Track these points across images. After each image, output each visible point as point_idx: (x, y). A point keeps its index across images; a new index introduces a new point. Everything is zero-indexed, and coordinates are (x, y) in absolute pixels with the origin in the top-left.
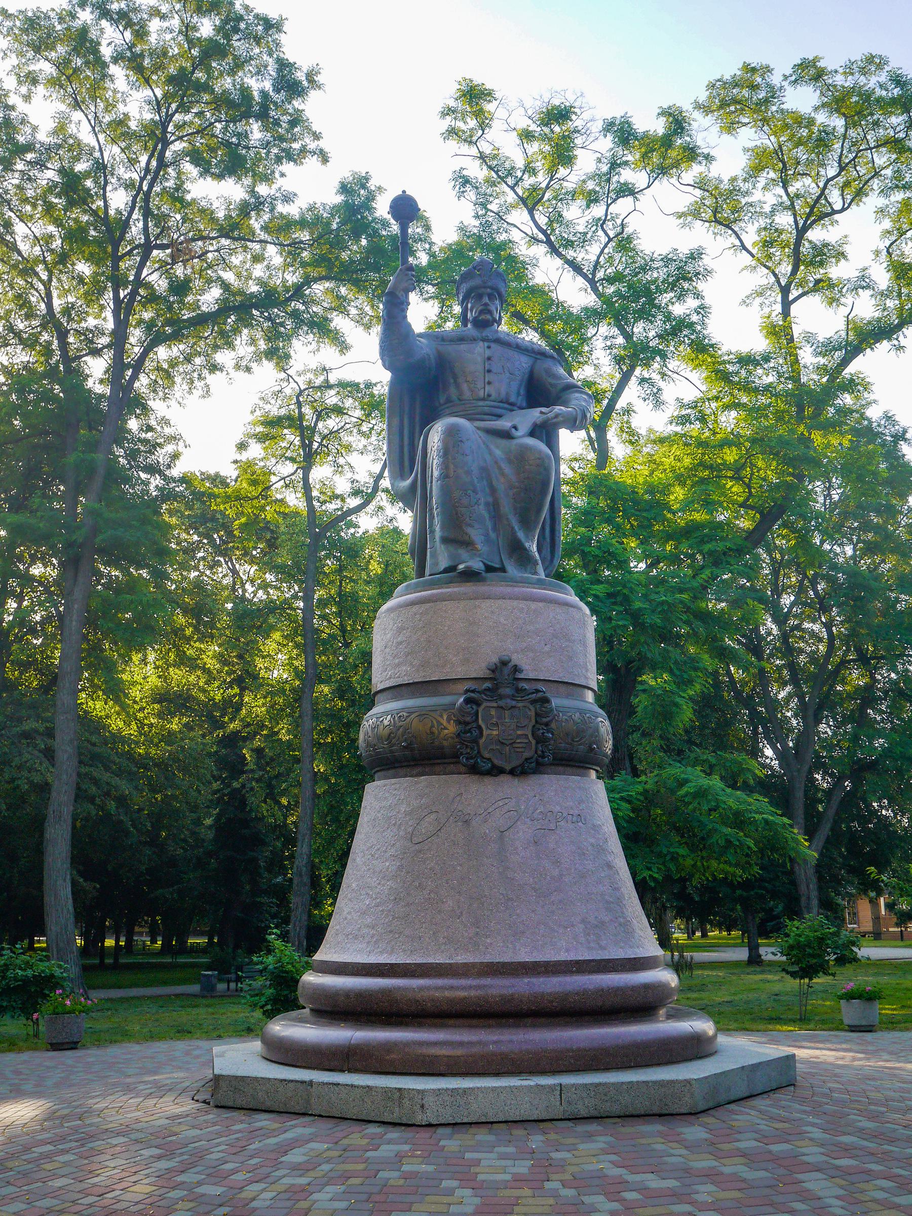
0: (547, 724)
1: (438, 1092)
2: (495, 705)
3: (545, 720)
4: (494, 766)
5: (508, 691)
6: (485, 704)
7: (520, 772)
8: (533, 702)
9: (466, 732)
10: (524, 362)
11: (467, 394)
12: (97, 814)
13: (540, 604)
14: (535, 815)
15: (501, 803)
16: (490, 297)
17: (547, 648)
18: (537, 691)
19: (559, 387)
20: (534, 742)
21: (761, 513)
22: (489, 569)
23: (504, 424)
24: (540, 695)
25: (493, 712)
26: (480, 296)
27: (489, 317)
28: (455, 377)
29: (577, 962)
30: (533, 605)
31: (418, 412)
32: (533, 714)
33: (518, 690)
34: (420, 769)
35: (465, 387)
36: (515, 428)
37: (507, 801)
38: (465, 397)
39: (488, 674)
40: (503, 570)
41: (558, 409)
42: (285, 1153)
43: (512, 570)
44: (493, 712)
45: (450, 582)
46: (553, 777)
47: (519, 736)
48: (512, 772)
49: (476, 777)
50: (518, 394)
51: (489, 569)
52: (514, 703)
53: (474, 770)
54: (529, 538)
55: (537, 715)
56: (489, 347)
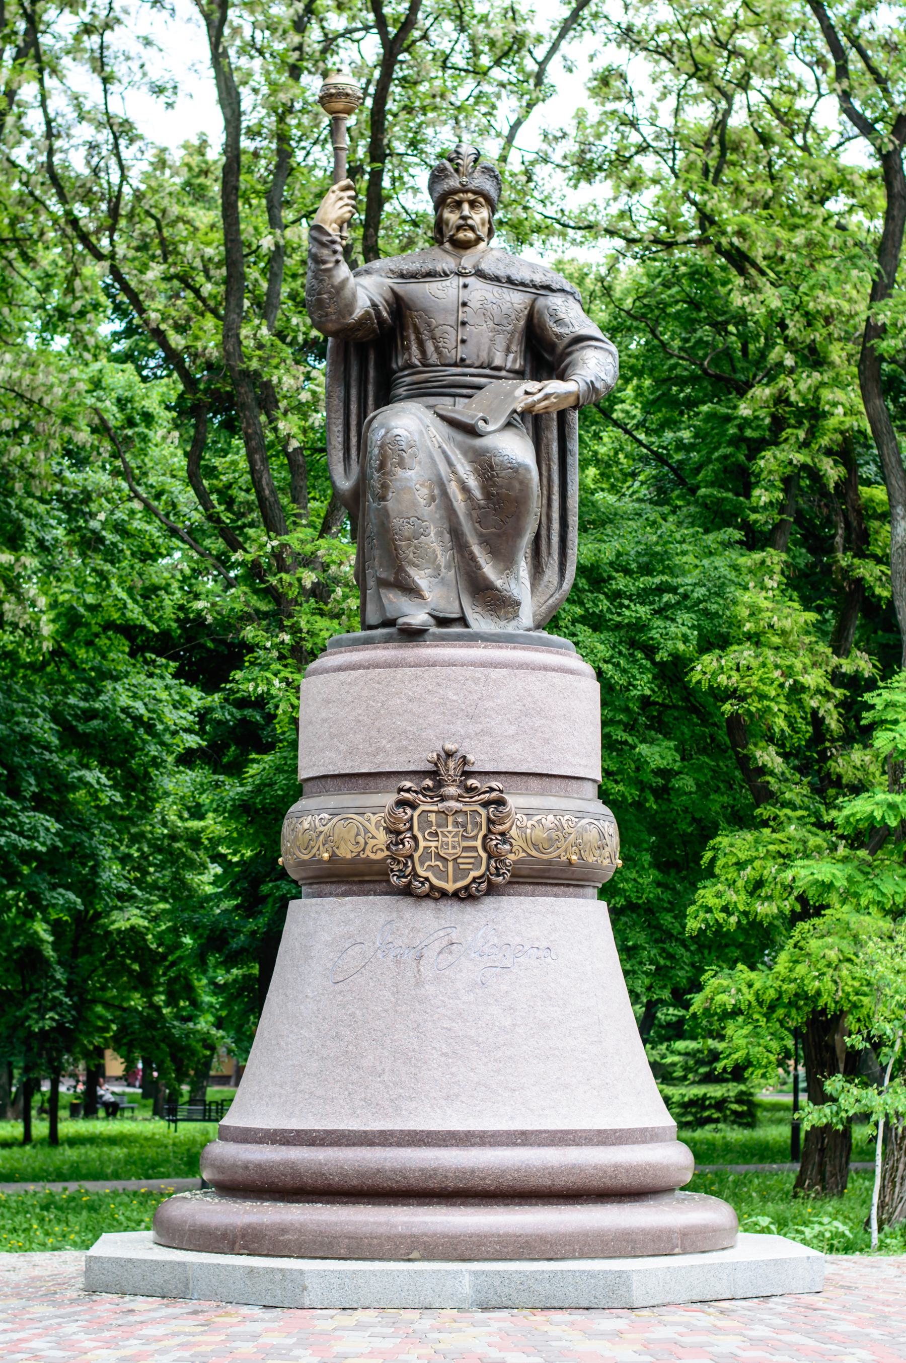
0: (503, 834)
1: (322, 1274)
2: (435, 808)
3: (500, 828)
4: (432, 887)
7: (465, 896)
8: (486, 804)
9: (397, 844)
10: (518, 300)
11: (433, 358)
13: (504, 671)
14: (486, 950)
15: (441, 933)
16: (473, 204)
17: (512, 730)
18: (492, 790)
19: (566, 341)
20: (484, 855)
24: (494, 795)
25: (433, 817)
26: (458, 204)
28: (417, 332)
29: (523, 1133)
30: (495, 674)
31: (372, 373)
32: (484, 820)
33: (470, 790)
34: (344, 888)
35: (430, 347)
38: (431, 361)
39: (430, 767)
40: (463, 621)
41: (555, 386)
43: (480, 622)
44: (433, 817)
45: (388, 639)
46: (514, 900)
47: (465, 849)
49: (409, 900)
50: (508, 351)
51: (442, 622)
53: (407, 892)
55: (490, 821)
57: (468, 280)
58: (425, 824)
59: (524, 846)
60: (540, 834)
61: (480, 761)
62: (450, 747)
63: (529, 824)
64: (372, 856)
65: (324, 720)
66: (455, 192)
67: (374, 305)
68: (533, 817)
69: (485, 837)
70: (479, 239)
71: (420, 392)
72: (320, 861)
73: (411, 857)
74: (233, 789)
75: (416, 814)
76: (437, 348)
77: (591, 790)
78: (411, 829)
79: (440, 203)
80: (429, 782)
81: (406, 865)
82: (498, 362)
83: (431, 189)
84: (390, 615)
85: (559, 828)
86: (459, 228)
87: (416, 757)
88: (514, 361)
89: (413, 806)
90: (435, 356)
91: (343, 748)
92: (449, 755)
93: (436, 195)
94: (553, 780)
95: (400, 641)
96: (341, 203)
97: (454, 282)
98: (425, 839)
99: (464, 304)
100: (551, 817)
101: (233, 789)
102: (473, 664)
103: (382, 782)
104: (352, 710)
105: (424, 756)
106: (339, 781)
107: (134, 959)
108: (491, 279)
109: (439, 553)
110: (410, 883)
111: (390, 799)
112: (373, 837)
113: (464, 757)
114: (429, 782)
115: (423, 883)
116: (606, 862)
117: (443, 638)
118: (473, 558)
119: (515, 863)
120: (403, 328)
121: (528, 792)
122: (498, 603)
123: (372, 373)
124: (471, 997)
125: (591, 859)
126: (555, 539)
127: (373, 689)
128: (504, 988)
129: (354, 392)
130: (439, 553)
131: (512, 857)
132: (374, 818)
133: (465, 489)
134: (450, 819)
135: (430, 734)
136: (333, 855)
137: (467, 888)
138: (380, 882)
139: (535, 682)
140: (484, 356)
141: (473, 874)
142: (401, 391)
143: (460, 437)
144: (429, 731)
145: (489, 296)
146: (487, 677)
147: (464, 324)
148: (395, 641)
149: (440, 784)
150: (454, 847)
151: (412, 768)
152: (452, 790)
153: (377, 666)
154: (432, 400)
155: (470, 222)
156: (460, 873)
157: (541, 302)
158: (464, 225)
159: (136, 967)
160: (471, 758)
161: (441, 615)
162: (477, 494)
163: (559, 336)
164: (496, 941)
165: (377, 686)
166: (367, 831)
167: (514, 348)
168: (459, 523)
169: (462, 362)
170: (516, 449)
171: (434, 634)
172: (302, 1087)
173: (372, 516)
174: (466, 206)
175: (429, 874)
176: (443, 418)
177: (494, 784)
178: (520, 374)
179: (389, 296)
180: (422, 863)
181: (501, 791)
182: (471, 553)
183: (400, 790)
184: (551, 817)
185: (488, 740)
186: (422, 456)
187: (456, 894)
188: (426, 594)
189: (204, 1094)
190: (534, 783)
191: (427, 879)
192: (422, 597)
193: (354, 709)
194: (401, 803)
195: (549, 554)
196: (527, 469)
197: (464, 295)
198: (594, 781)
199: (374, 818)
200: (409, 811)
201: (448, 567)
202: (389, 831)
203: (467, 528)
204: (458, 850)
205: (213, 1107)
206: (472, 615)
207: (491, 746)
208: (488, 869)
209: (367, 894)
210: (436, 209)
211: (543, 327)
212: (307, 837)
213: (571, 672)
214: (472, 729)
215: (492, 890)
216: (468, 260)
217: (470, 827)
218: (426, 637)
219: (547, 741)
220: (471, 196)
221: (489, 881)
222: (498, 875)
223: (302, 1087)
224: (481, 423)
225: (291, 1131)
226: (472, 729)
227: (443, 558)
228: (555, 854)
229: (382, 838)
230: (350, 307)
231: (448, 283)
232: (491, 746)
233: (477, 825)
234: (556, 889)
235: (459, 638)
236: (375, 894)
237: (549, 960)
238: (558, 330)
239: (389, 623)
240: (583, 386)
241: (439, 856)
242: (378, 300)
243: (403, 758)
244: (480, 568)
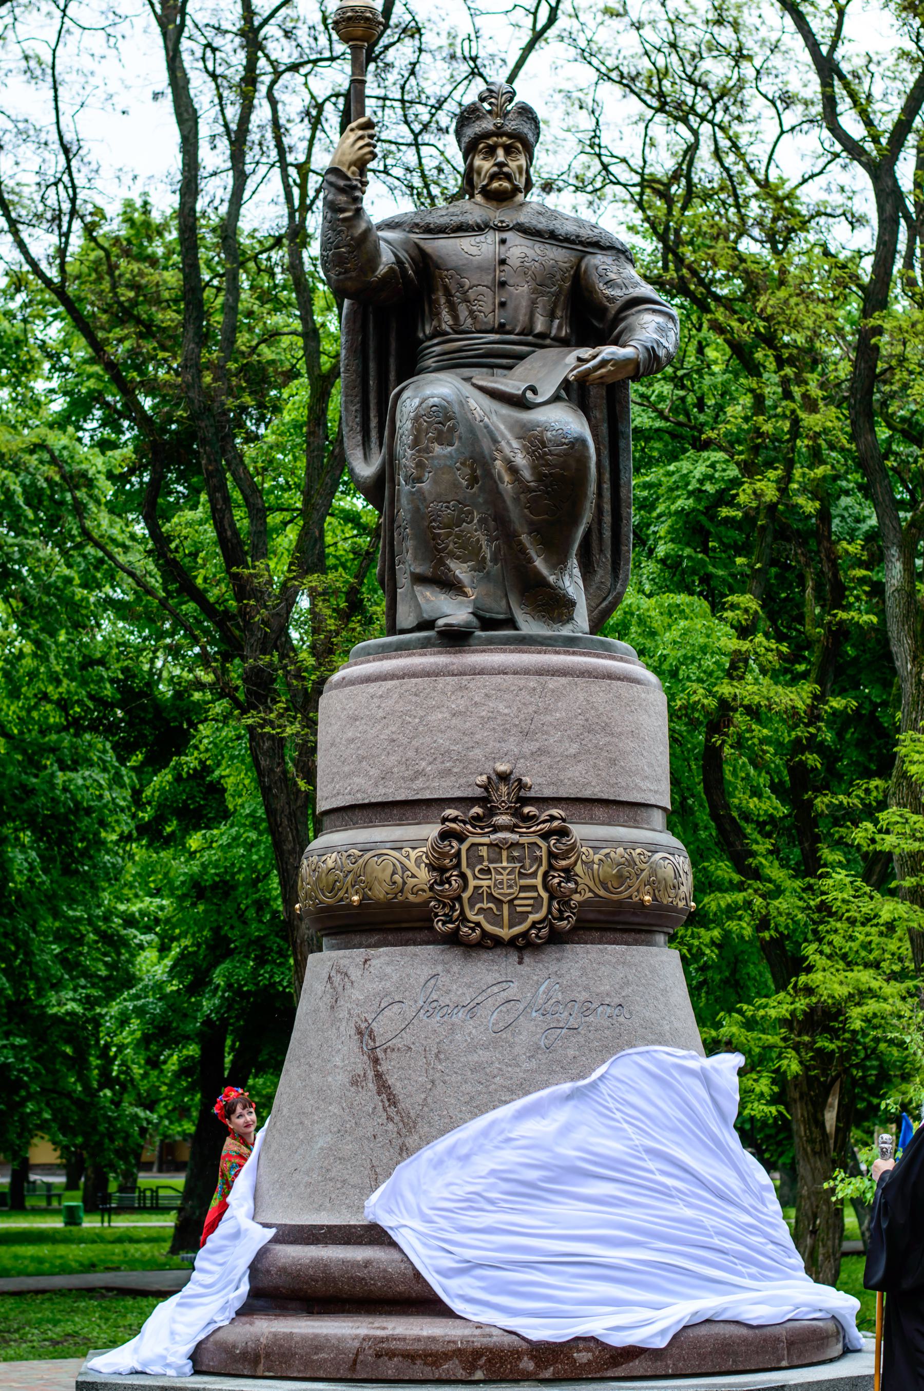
2: (485, 840)
5: (503, 819)
6: (472, 840)
7: (522, 946)
8: (545, 836)
9: (442, 883)
12: (131, 428)
13: (563, 680)
15: (495, 989)
16: (508, 150)
17: (574, 749)
18: (552, 818)
19: (619, 303)
20: (545, 895)
21: (184, 845)
22: (487, 623)
24: (556, 823)
25: (484, 851)
28: (448, 293)
30: (554, 683)
36: (534, 390)
37: (504, 985)
39: (479, 792)
40: (511, 623)
41: (608, 351)
43: (529, 626)
44: (484, 851)
45: (425, 644)
46: (579, 948)
47: (523, 888)
49: (457, 951)
50: (552, 316)
52: (515, 837)
53: (453, 940)
54: (559, 563)
55: (551, 855)
56: (503, 241)
57: (505, 235)
58: (474, 858)
59: (591, 884)
61: (538, 781)
62: (502, 767)
63: (597, 858)
64: (411, 898)
65: (352, 741)
66: (487, 135)
67: (399, 261)
69: (546, 874)
70: (516, 190)
71: (453, 362)
72: (350, 905)
73: (459, 898)
75: (464, 847)
76: (471, 312)
77: (658, 819)
78: (458, 865)
79: (469, 151)
80: (477, 810)
81: (453, 909)
83: (458, 134)
85: (631, 863)
87: (462, 781)
88: (560, 328)
89: (461, 838)
90: (469, 321)
91: (373, 772)
92: (504, 777)
93: (465, 140)
95: (441, 645)
96: (361, 143)
97: (490, 240)
98: (475, 877)
99: (503, 262)
100: (620, 850)
103: (422, 812)
104: (393, 721)
106: (369, 813)
107: (68, 1042)
108: (532, 234)
109: (484, 543)
110: (458, 928)
111: (432, 831)
112: (414, 876)
113: (520, 780)
115: (473, 929)
116: (681, 904)
117: (490, 641)
118: (523, 550)
119: (581, 904)
120: (432, 290)
122: (555, 607)
123: (393, 345)
124: (533, 1064)
125: (666, 901)
126: (607, 534)
127: (410, 702)
128: (571, 1053)
129: (372, 365)
130: (484, 543)
131: (576, 897)
132: (413, 854)
133: (513, 470)
136: (365, 897)
137: (525, 934)
138: (421, 929)
141: (533, 917)
142: (430, 362)
143: (506, 410)
144: (477, 751)
145: (530, 252)
147: (503, 284)
148: (434, 646)
149: (491, 812)
150: (510, 887)
151: (458, 794)
152: (503, 819)
153: (414, 674)
154: (467, 372)
155: (505, 169)
156: (517, 918)
158: (500, 173)
159: (69, 1050)
160: (527, 780)
161: (488, 615)
162: (527, 474)
163: (612, 300)
165: (414, 699)
166: (405, 868)
167: (559, 313)
168: (506, 509)
169: (501, 329)
170: (566, 422)
171: (479, 637)
172: (333, 1174)
173: (404, 501)
174: (500, 152)
175: (480, 918)
176: (482, 389)
177: (555, 812)
178: (564, 343)
179: (414, 253)
180: (472, 907)
181: (564, 820)
182: (520, 543)
183: (445, 820)
184: (620, 850)
185: (547, 760)
186: (462, 429)
188: (468, 590)
189: (135, 1181)
190: (599, 812)
191: (478, 924)
193: (388, 726)
194: (445, 835)
195: (601, 551)
197: (503, 252)
198: (664, 809)
199: (413, 854)
200: (455, 844)
201: (495, 560)
202: (431, 867)
203: (514, 513)
204: (515, 889)
205: (148, 1193)
206: (520, 616)
207: (551, 767)
208: (549, 911)
209: (406, 943)
210: (465, 158)
212: (331, 878)
213: (637, 681)
215: (557, 938)
217: (528, 861)
218: (472, 641)
219: (613, 762)
221: (551, 926)
222: (561, 919)
223: (333, 1174)
224: (529, 395)
225: (321, 1227)
228: (626, 894)
229: (424, 876)
231: (482, 238)
232: (551, 767)
233: (539, 860)
235: (507, 641)
236: (415, 943)
237: (621, 1019)
238: (609, 292)
239: (426, 625)
240: (643, 355)
241: (491, 898)
242: (403, 255)
243: (447, 782)
244: (530, 561)
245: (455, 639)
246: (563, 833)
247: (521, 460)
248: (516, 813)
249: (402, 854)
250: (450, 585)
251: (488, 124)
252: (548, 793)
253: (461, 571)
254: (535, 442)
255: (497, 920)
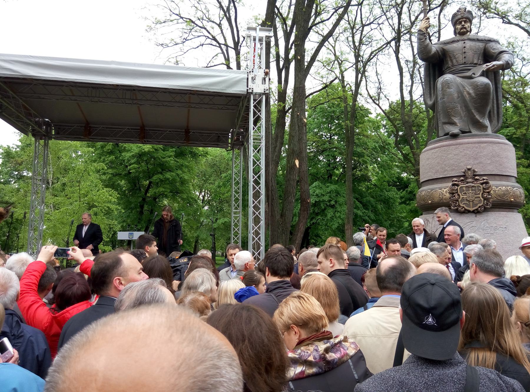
0: (488, 192)
4: (465, 209)
5: (470, 180)
7: (476, 212)
8: (482, 184)
10: (481, 45)
13: (485, 144)
15: (469, 224)
16: (465, 22)
18: (484, 179)
20: (482, 199)
22: (463, 132)
23: (469, 74)
24: (485, 181)
25: (464, 189)
26: (461, 23)
27: (465, 30)
28: (450, 57)
30: (482, 145)
32: (482, 188)
33: (477, 180)
39: (462, 174)
40: (470, 132)
42: (5, 97)
43: (474, 132)
44: (464, 189)
45: (446, 139)
48: (473, 212)
50: (478, 59)
52: (473, 185)
55: (484, 189)
56: (464, 43)
58: (462, 190)
60: (501, 193)
62: (469, 167)
65: (428, 164)
66: (460, 19)
67: (437, 51)
68: (498, 187)
69: (482, 194)
73: (458, 201)
74: (408, 207)
78: (457, 192)
80: (462, 178)
81: (456, 203)
82: (475, 62)
84: (446, 132)
85: (507, 190)
86: (461, 29)
89: (458, 185)
92: (469, 169)
94: (503, 177)
100: (504, 187)
101: (408, 207)
102: (475, 143)
105: (460, 171)
111: (450, 184)
114: (462, 178)
118: (473, 114)
119: (493, 201)
121: (495, 180)
122: (482, 127)
126: (496, 112)
132: (445, 190)
134: (470, 189)
135: (462, 164)
137: (477, 209)
139: (496, 147)
140: (471, 60)
146: (480, 146)
157: (488, 45)
162: (473, 95)
164: (488, 225)
170: (485, 80)
174: (463, 23)
177: (484, 178)
180: (461, 203)
184: (504, 187)
187: (473, 212)
190: (497, 177)
191: (463, 207)
192: (457, 125)
194: (453, 185)
196: (489, 84)
199: (445, 190)
202: (450, 193)
206: (472, 130)
211: (489, 52)
214: (476, 162)
216: (465, 37)
220: (464, 19)
226: (476, 162)
227: (463, 114)
230: (430, 51)
234: (506, 210)
235: (469, 136)
241: (467, 200)
244: (475, 116)
245: (454, 136)
246: (487, 183)
247: (471, 91)
248: (473, 178)
249: (443, 190)
250: (453, 124)
251: (459, 17)
252: (482, 173)
253: (456, 120)
254: (476, 87)
255: (469, 206)
